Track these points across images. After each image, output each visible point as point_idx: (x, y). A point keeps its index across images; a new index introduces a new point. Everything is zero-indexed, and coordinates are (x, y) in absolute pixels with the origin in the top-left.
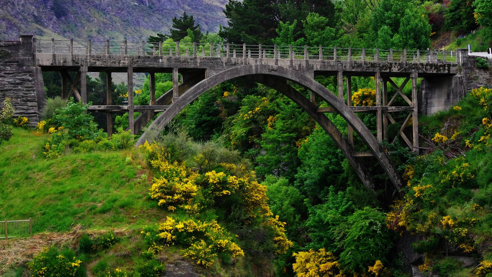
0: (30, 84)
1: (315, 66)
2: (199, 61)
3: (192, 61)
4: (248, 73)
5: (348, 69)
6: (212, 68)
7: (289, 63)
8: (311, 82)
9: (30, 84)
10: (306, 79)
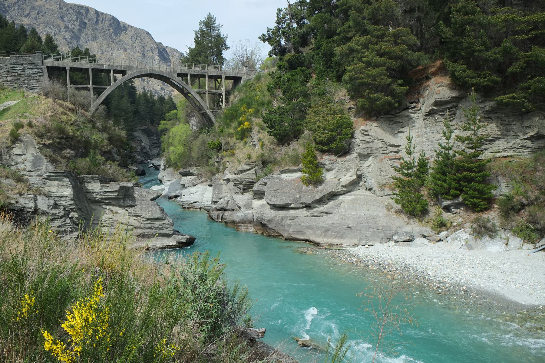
0: (41, 74)
4: (146, 73)
7: (165, 69)
9: (41, 74)
10: (173, 77)
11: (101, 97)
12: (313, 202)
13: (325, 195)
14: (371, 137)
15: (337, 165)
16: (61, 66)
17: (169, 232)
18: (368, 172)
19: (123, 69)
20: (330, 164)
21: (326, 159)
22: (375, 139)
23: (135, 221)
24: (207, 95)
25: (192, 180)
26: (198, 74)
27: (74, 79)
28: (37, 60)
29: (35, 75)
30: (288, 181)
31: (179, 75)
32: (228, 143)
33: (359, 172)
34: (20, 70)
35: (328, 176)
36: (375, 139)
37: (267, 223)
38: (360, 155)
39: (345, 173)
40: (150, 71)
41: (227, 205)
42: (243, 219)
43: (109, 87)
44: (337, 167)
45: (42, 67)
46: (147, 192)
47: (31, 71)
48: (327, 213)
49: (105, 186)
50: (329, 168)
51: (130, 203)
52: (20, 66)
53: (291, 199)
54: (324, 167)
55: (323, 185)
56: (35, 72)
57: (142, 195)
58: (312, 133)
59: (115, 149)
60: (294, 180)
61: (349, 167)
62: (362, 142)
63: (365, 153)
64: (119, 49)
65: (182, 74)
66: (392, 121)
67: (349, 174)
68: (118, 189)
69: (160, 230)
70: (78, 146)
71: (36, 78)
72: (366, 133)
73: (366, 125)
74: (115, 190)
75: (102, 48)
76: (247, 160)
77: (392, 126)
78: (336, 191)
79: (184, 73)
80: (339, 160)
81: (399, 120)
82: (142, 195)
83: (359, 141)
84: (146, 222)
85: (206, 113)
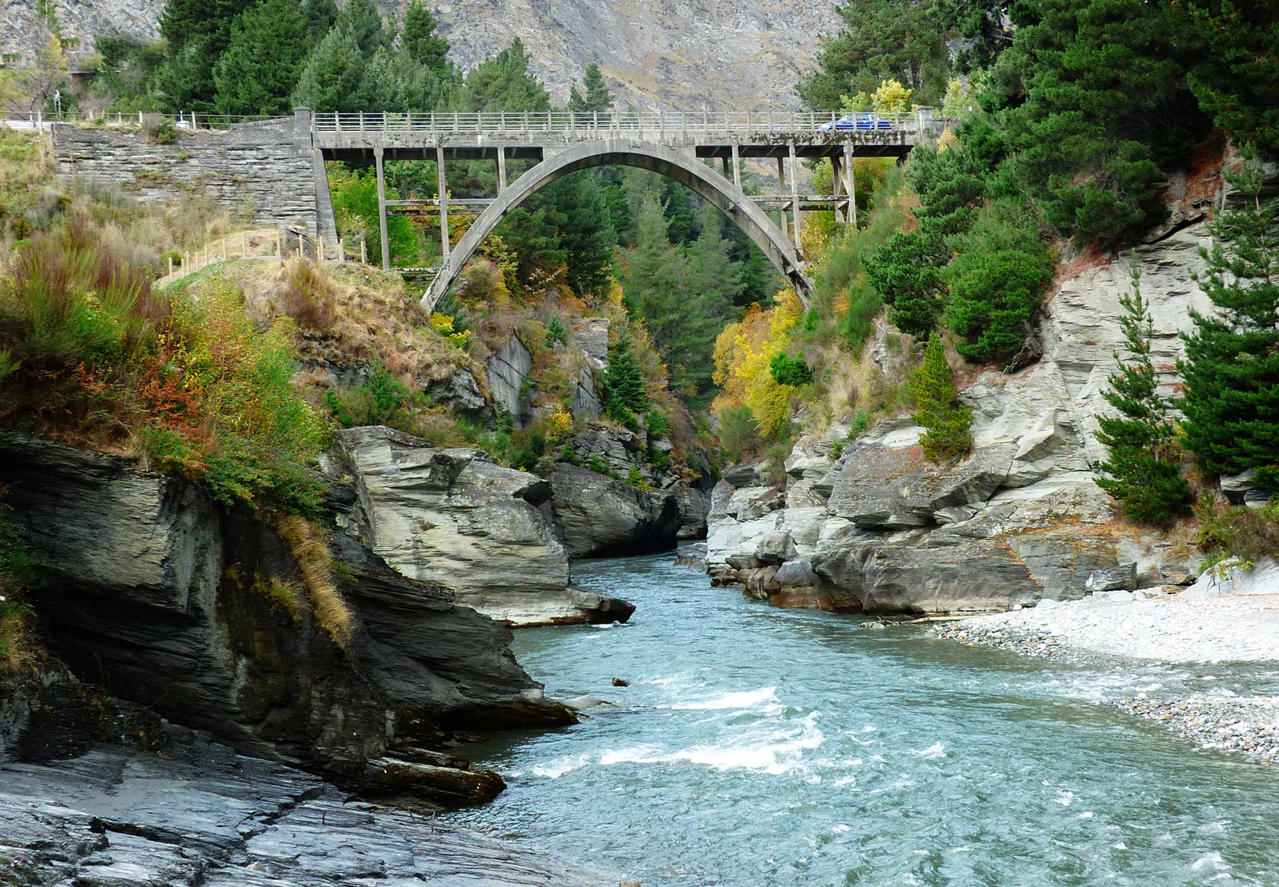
0: (307, 173)
1: (696, 140)
2: (531, 137)
3: (523, 137)
5: (747, 142)
6: (550, 146)
7: (658, 137)
8: (692, 164)
9: (307, 173)
11: (472, 233)
12: (936, 505)
13: (966, 485)
14: (1092, 313)
15: (1004, 399)
16: (361, 146)
17: (557, 580)
18: (1085, 415)
19: (530, 143)
20: (990, 395)
21: (981, 385)
22: (1103, 318)
23: (473, 549)
24: (796, 213)
25: (759, 499)
26: (762, 144)
27: (470, 174)
28: (296, 135)
29: (293, 177)
30: (896, 454)
31: (703, 152)
32: (822, 363)
33: (1062, 418)
34: (255, 163)
35: (986, 435)
36: (1103, 318)
37: (829, 573)
38: (1062, 365)
39: (1028, 421)
40: (612, 145)
41: (785, 547)
42: (795, 575)
43: (491, 201)
44: (1008, 402)
45: (310, 151)
46: (504, 475)
47: (282, 166)
48: (969, 536)
49: (402, 455)
50: (990, 408)
51: (462, 500)
52: (254, 153)
53: (888, 500)
54: (979, 408)
55: (973, 457)
56: (291, 169)
57: (491, 483)
58: (128, 218)
59: (466, 378)
60: (908, 448)
61: (1035, 403)
62: (1066, 327)
63: (1073, 358)
64: (742, 19)
65: (714, 147)
66: (1154, 262)
67: (1039, 423)
68: (428, 461)
69: (534, 573)
70: (356, 361)
71: (295, 185)
72: (1075, 301)
73: (1077, 277)
74: (422, 463)
75: (669, 23)
76: (847, 408)
77: (1156, 277)
78: (1004, 473)
79: (718, 143)
80: (1012, 383)
81: (1169, 256)
82: (491, 483)
83: (1058, 325)
84: (498, 551)
85: (795, 271)
